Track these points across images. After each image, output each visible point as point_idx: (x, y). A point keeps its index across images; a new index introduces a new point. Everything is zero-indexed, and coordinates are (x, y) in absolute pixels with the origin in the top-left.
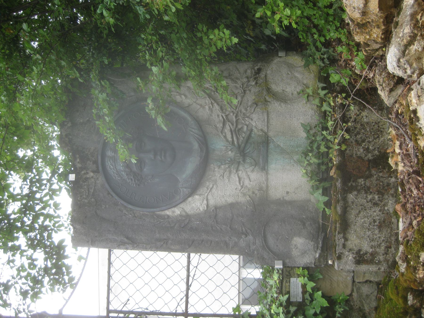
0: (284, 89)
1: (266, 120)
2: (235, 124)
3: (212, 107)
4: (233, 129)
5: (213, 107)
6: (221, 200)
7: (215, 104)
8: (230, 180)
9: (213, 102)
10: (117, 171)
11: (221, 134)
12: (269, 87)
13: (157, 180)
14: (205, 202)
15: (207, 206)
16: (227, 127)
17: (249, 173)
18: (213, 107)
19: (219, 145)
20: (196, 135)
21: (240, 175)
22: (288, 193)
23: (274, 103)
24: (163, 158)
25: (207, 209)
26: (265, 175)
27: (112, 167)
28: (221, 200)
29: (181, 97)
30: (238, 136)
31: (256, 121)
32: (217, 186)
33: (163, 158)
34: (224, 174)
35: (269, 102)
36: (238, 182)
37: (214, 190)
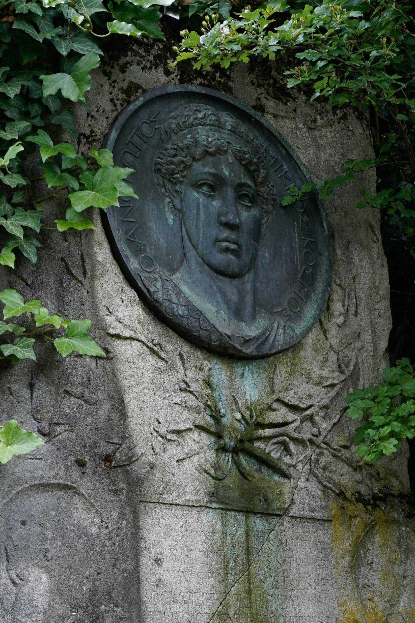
0: (374, 566)
1: (313, 515)
2: (297, 435)
3: (325, 384)
4: (288, 428)
5: (324, 387)
6: (131, 376)
7: (333, 393)
8: (177, 408)
9: (336, 389)
10: (192, 125)
11: (275, 397)
12: (377, 527)
13: (170, 219)
14: (127, 333)
15: (118, 337)
16: (291, 416)
17: (196, 458)
18: (324, 387)
19: (250, 387)
20: (273, 333)
21: (190, 433)
22: (158, 561)
23: (348, 538)
24: (225, 244)
25: (109, 334)
26: (197, 501)
27: (200, 115)
28: (131, 376)
29: (341, 314)
30: (274, 440)
31: (301, 491)
32: (162, 372)
33: (225, 244)
34: (191, 392)
35: (350, 526)
36: (176, 428)
37: (153, 362)
